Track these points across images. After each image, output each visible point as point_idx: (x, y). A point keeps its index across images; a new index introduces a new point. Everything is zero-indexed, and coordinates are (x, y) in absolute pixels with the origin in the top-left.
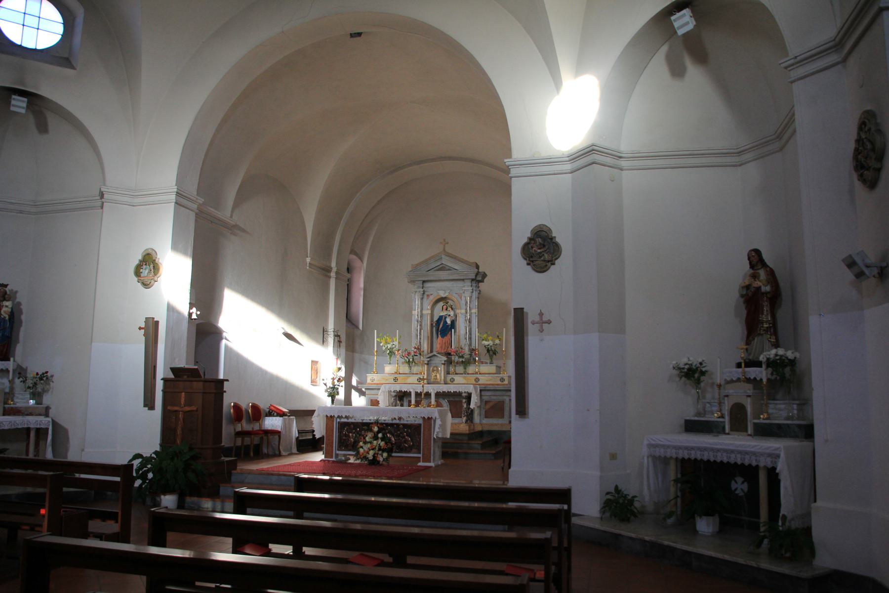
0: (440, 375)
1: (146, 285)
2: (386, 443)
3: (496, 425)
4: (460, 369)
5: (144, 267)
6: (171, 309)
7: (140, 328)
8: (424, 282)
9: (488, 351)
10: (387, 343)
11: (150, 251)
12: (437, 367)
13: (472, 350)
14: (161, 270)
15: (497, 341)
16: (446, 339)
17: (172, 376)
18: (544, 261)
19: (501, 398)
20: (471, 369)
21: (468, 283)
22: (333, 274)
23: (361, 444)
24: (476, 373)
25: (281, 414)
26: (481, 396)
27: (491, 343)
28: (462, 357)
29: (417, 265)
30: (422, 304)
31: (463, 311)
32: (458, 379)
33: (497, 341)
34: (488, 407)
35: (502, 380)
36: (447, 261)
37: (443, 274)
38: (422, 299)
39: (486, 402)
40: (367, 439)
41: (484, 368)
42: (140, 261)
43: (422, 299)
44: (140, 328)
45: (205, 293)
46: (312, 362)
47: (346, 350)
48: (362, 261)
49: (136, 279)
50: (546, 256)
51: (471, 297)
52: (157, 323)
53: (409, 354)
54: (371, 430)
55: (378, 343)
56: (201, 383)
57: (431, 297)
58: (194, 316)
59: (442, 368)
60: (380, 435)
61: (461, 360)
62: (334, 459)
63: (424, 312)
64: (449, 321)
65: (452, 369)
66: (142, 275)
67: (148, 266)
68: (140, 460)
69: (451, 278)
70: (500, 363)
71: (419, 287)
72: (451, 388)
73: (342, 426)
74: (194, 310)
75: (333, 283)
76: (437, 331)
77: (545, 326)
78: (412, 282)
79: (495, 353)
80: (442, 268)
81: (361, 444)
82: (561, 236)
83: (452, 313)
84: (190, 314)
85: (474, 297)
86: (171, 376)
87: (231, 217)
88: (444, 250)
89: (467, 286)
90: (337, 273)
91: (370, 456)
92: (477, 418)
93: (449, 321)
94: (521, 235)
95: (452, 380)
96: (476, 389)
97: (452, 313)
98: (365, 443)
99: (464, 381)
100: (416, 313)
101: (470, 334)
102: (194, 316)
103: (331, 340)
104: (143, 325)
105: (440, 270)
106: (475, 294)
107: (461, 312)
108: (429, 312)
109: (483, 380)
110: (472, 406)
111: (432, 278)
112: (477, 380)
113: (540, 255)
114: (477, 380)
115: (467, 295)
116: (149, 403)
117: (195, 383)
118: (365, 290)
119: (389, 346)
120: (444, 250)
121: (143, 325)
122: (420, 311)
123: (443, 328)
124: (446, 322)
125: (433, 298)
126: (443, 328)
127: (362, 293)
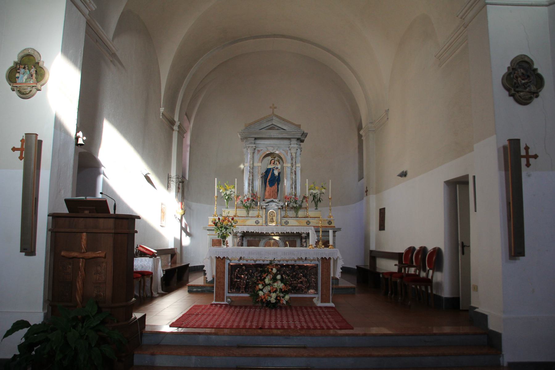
0: (278, 217)
1: (24, 95)
2: (285, 284)
5: (22, 71)
6: (58, 126)
7: (14, 149)
8: (256, 139)
10: (226, 190)
11: (32, 52)
13: (305, 197)
14: (47, 76)
15: (323, 190)
17: (65, 210)
18: (530, 92)
20: (301, 213)
21: (294, 142)
22: (176, 128)
23: (260, 286)
24: (307, 217)
25: (152, 255)
29: (250, 124)
31: (289, 165)
33: (323, 190)
36: (276, 122)
37: (274, 133)
40: (267, 281)
42: (16, 64)
44: (14, 149)
45: (89, 119)
48: (189, 122)
49: (8, 87)
50: (533, 88)
52: (40, 142)
54: (269, 273)
55: (218, 191)
56: (112, 221)
57: (261, 153)
58: (80, 141)
60: (279, 277)
62: (225, 303)
63: (256, 164)
66: (18, 81)
67: (27, 71)
68: (26, 330)
69: (280, 136)
71: (251, 143)
72: (288, 229)
73: (233, 268)
74: (80, 134)
77: (532, 161)
78: (245, 138)
79: (319, 200)
81: (260, 286)
82: (542, 66)
83: (279, 166)
84: (77, 138)
86: (64, 210)
87: (113, 40)
88: (273, 113)
90: (179, 127)
91: (273, 300)
94: (501, 67)
95: (286, 223)
98: (265, 285)
99: (297, 224)
102: (80, 141)
103: (173, 186)
104: (19, 146)
105: (270, 129)
107: (288, 165)
111: (264, 136)
113: (525, 86)
116: (28, 247)
117: (101, 220)
119: (228, 193)
120: (273, 113)
121: (19, 146)
123: (272, 180)
126: (272, 180)
127: (189, 149)
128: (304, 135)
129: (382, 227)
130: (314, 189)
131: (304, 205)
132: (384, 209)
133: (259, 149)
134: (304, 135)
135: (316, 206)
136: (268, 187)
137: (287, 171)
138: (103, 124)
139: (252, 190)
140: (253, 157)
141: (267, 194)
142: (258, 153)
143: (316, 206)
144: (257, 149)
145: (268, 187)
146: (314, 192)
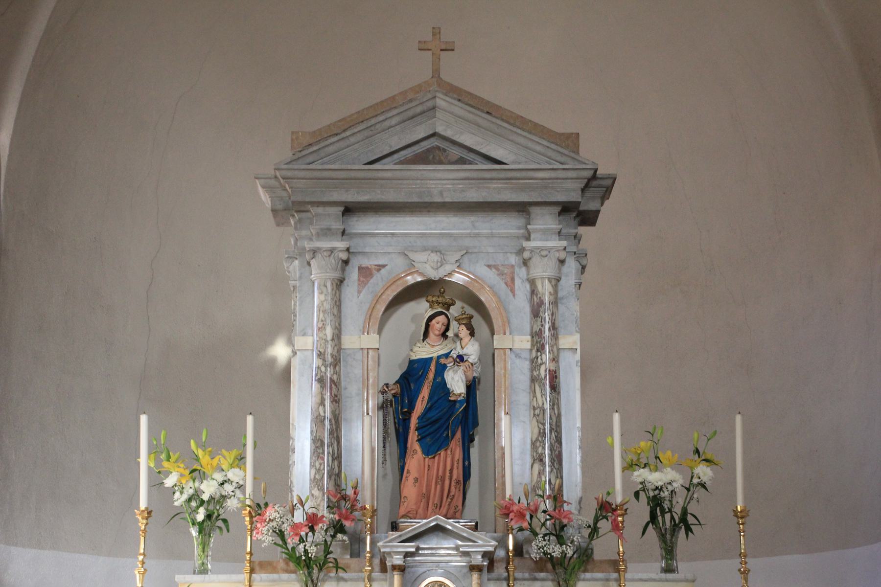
8: (349, 210)
10: (197, 474)
13: (605, 508)
15: (704, 472)
21: (545, 220)
30: (338, 304)
31: (523, 342)
33: (704, 472)
36: (451, 123)
37: (441, 181)
51: (556, 281)
57: (378, 281)
64: (456, 382)
69: (473, 195)
71: (327, 232)
79: (684, 523)
80: (432, 152)
83: (472, 350)
88: (436, 73)
89: (546, 234)
93: (456, 382)
105: (422, 159)
111: (390, 196)
119: (208, 489)
120: (436, 73)
123: (434, 418)
124: (441, 389)
125: (383, 286)
126: (434, 418)
128: (598, 185)
130: (656, 463)
131: (602, 548)
134: (598, 185)
135: (669, 552)
136: (416, 459)
137: (514, 374)
139: (336, 475)
140: (338, 304)
141: (410, 490)
143: (669, 552)
144: (356, 262)
145: (416, 459)
146: (655, 478)
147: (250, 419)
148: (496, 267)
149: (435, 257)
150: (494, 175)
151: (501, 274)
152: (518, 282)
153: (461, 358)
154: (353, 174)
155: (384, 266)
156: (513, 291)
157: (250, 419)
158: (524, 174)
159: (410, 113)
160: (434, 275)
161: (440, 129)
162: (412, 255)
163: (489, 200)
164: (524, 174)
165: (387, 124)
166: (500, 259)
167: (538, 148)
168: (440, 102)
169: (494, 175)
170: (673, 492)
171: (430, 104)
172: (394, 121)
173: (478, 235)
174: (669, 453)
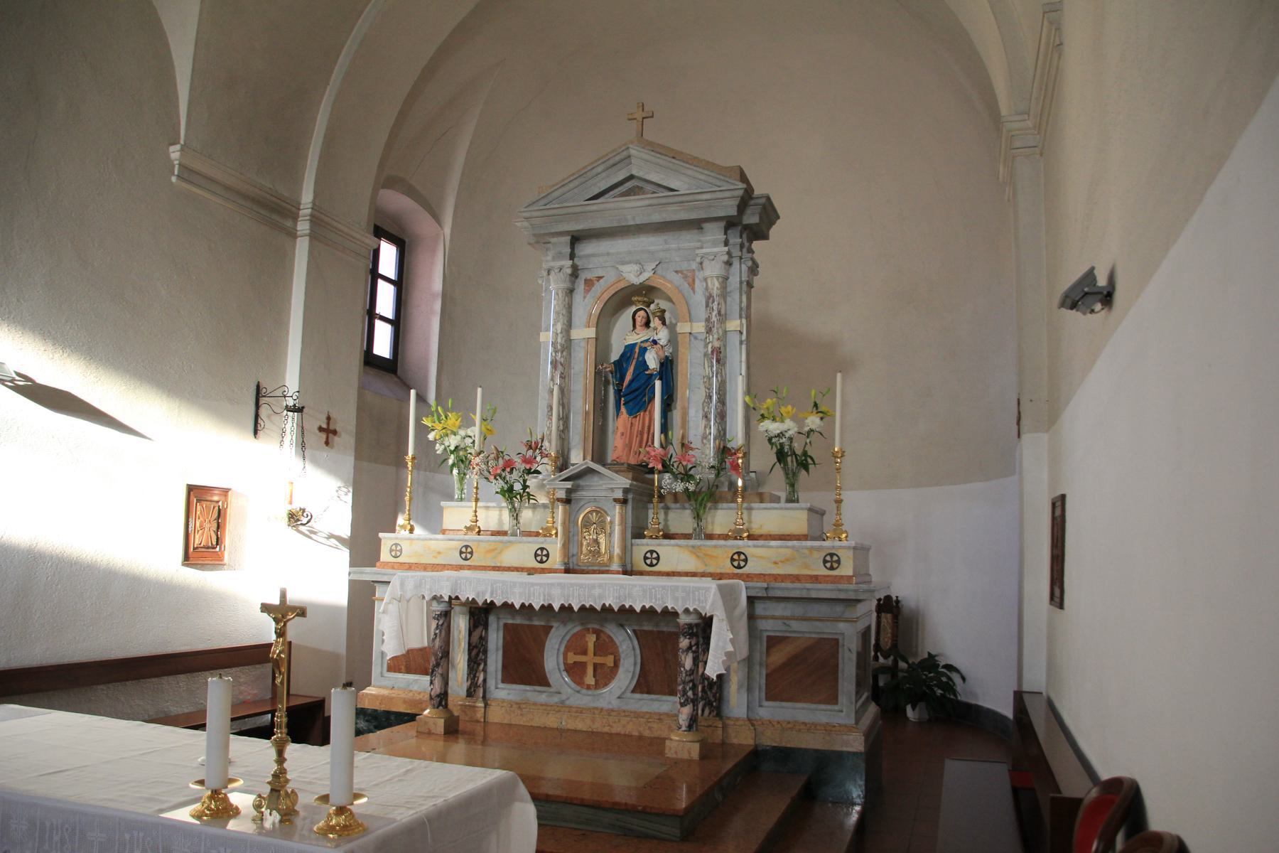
3: (811, 727)
4: (681, 519)
8: (576, 239)
9: (781, 456)
12: (600, 512)
15: (813, 421)
16: (637, 423)
19: (827, 630)
20: (722, 519)
21: (715, 233)
22: (303, 226)
24: (737, 536)
26: (752, 617)
27: (789, 426)
28: (687, 477)
31: (699, 327)
32: (673, 555)
33: (813, 421)
34: (779, 657)
35: (832, 560)
36: (644, 166)
37: (632, 209)
38: (571, 292)
39: (773, 642)
41: (767, 518)
43: (571, 292)
46: (191, 489)
47: (359, 457)
48: (437, 218)
53: (509, 466)
55: (422, 430)
57: (598, 288)
59: (615, 515)
61: (679, 487)
64: (652, 360)
65: (654, 516)
69: (656, 218)
70: (822, 499)
71: (558, 256)
75: (302, 249)
76: (618, 393)
79: (804, 462)
80: (631, 186)
83: (663, 335)
85: (734, 281)
89: (711, 247)
90: (315, 220)
92: (736, 702)
93: (652, 360)
95: (652, 558)
96: (727, 596)
97: (663, 335)
99: (691, 564)
100: (548, 337)
101: (722, 401)
106: (738, 273)
108: (591, 332)
109: (762, 559)
110: (713, 668)
111: (598, 224)
112: (739, 559)
114: (739, 559)
115: (713, 269)
118: (445, 296)
119: (453, 442)
122: (557, 331)
123: (633, 384)
125: (604, 290)
127: (438, 306)
129: (1057, 596)
132: (1063, 497)
133: (589, 275)
138: (293, 265)
140: (569, 308)
142: (587, 291)
144: (583, 276)
147: (479, 390)
148: (681, 272)
149: (636, 267)
150: (671, 200)
151: (685, 277)
152: (697, 281)
153: (655, 342)
154: (570, 210)
155: (601, 278)
156: (693, 289)
157: (479, 390)
158: (691, 198)
159: (611, 162)
160: (637, 281)
161: (635, 172)
162: (622, 268)
163: (668, 219)
164: (691, 198)
165: (595, 171)
166: (684, 266)
167: (703, 177)
168: (632, 152)
169: (671, 200)
170: (791, 439)
171: (625, 153)
172: (599, 169)
173: (668, 250)
174: (789, 407)
